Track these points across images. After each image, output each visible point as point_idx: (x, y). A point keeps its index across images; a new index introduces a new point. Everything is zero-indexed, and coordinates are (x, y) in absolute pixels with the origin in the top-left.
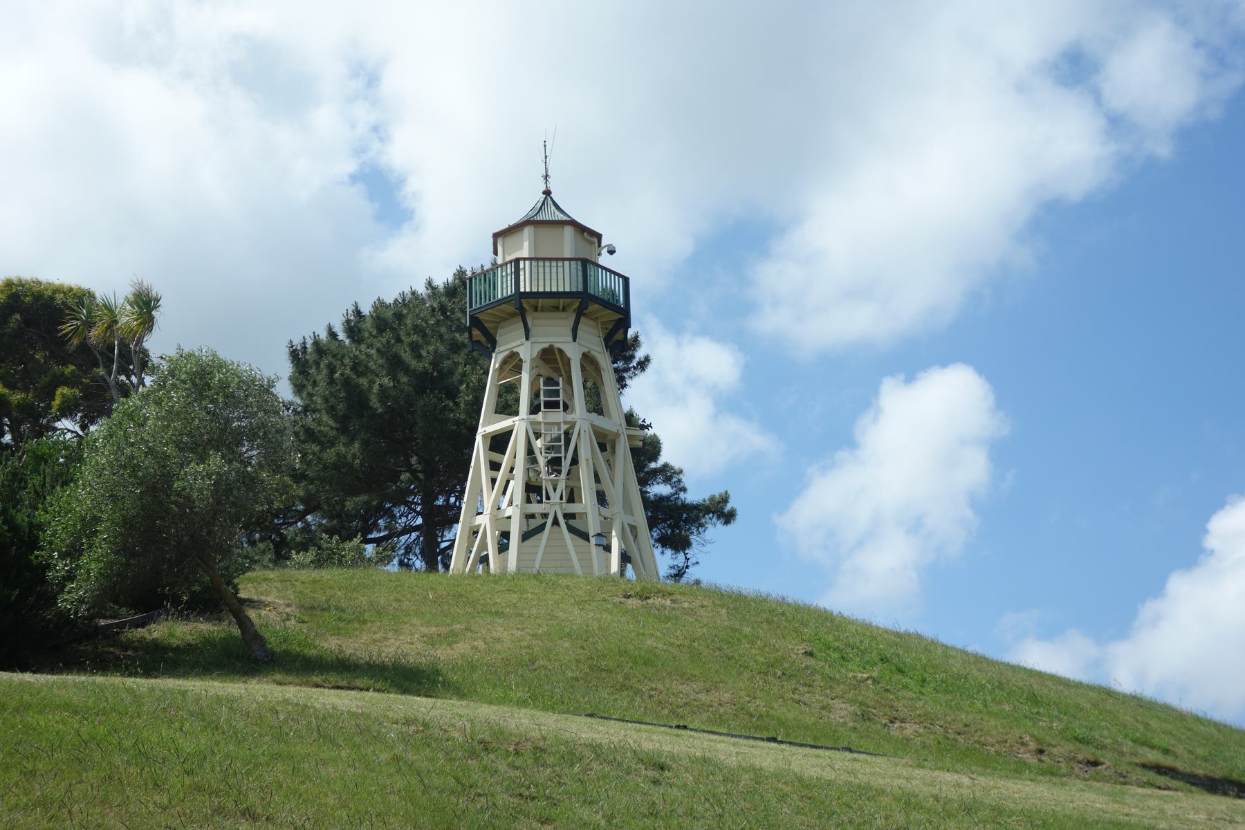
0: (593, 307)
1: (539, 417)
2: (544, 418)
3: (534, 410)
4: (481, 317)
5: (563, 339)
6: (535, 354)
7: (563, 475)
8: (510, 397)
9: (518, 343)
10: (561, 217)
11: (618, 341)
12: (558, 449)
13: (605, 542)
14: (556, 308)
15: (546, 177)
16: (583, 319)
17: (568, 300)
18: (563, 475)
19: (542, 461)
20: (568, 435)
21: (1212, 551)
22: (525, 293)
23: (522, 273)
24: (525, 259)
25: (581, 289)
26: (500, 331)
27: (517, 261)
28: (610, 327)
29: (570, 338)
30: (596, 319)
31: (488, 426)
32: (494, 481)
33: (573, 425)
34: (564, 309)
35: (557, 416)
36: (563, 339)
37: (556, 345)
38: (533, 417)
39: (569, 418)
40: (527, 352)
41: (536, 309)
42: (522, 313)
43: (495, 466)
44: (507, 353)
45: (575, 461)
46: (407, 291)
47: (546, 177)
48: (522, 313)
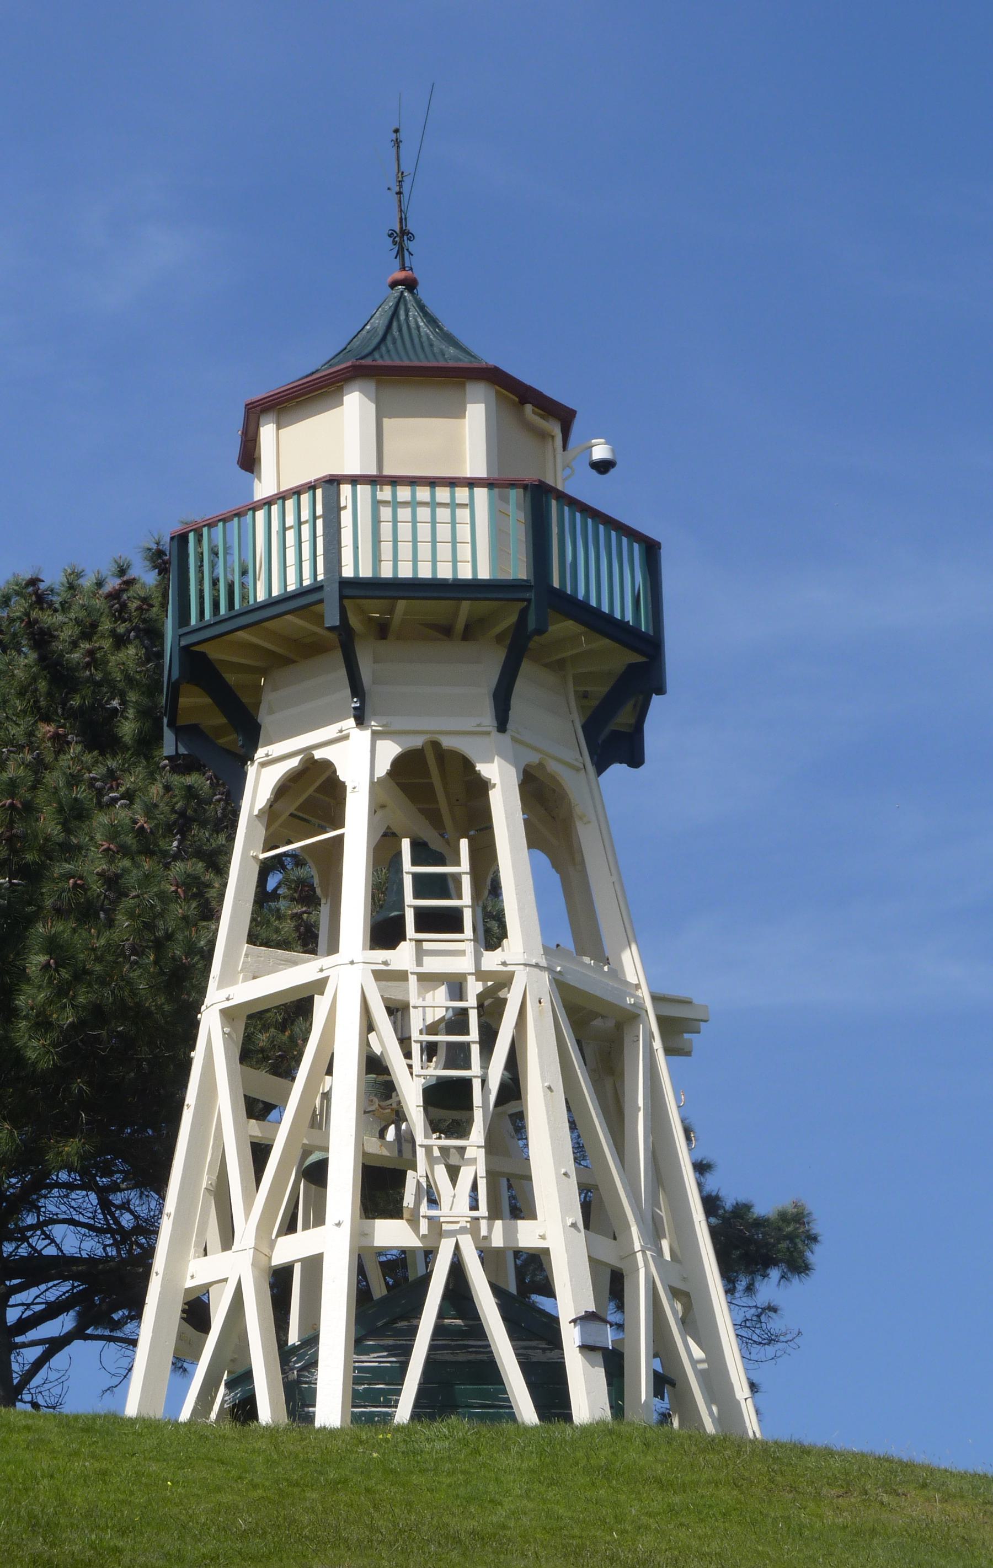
0: (563, 627)
1: (402, 957)
2: (420, 954)
3: (385, 933)
4: (214, 653)
5: (469, 724)
6: (383, 769)
7: (477, 1134)
8: (512, 1107)
9: (330, 732)
10: (465, 362)
11: (615, 734)
12: (458, 1056)
13: (609, 1337)
14: (446, 631)
15: (401, 237)
16: (526, 667)
17: (484, 607)
18: (477, 1134)
19: (411, 1093)
20: (491, 1009)
21: (134, 579)
22: (356, 583)
23: (346, 517)
24: (354, 480)
25: (519, 570)
26: (268, 698)
27: (333, 482)
28: (601, 690)
29: (488, 720)
30: (559, 666)
31: (238, 980)
32: (260, 1153)
33: (503, 981)
34: (468, 634)
35: (457, 954)
36: (469, 724)
37: (447, 742)
38: (381, 955)
39: (491, 961)
40: (359, 757)
41: (382, 630)
42: (346, 639)
43: (258, 1108)
44: (294, 762)
45: (512, 1090)
46: (816, 1229)
47: (401, 237)
48: (346, 639)
